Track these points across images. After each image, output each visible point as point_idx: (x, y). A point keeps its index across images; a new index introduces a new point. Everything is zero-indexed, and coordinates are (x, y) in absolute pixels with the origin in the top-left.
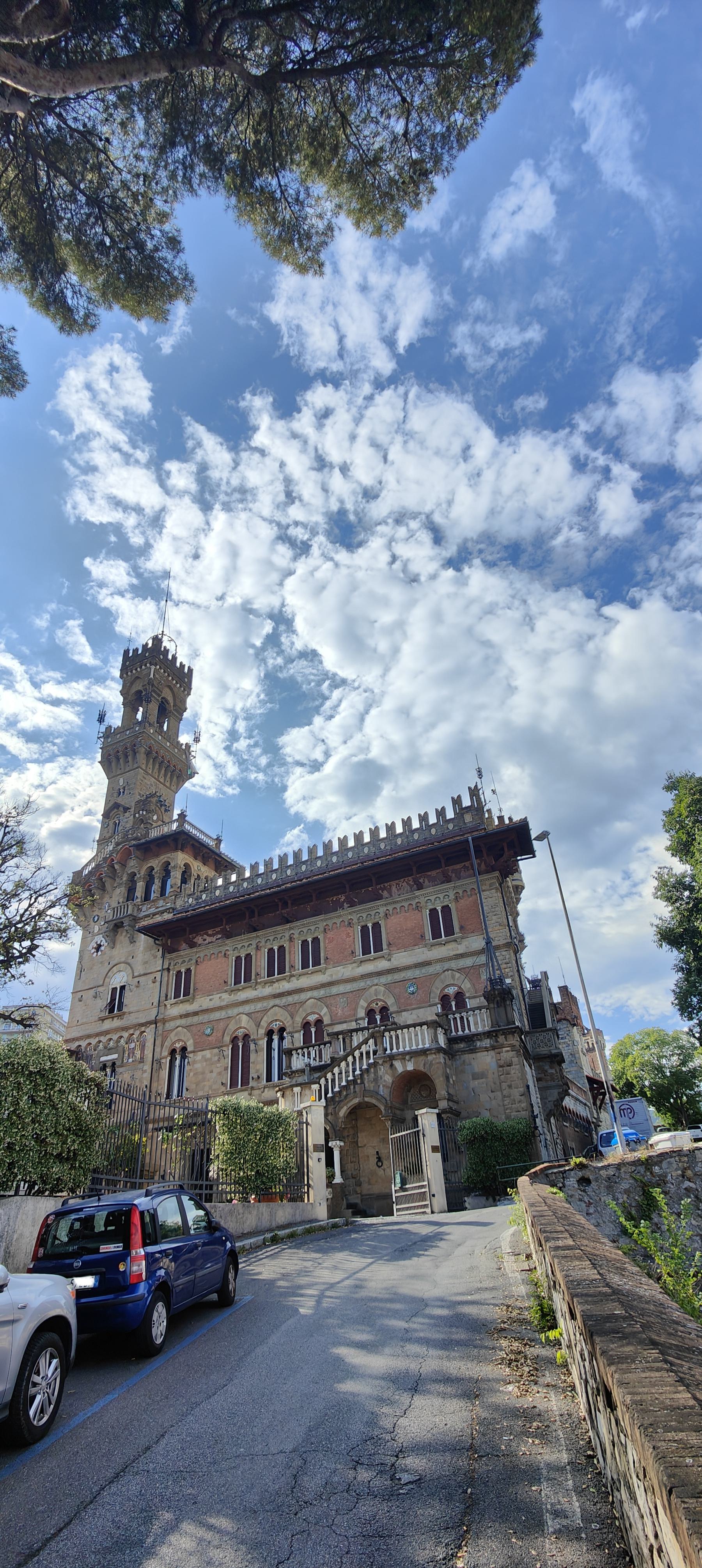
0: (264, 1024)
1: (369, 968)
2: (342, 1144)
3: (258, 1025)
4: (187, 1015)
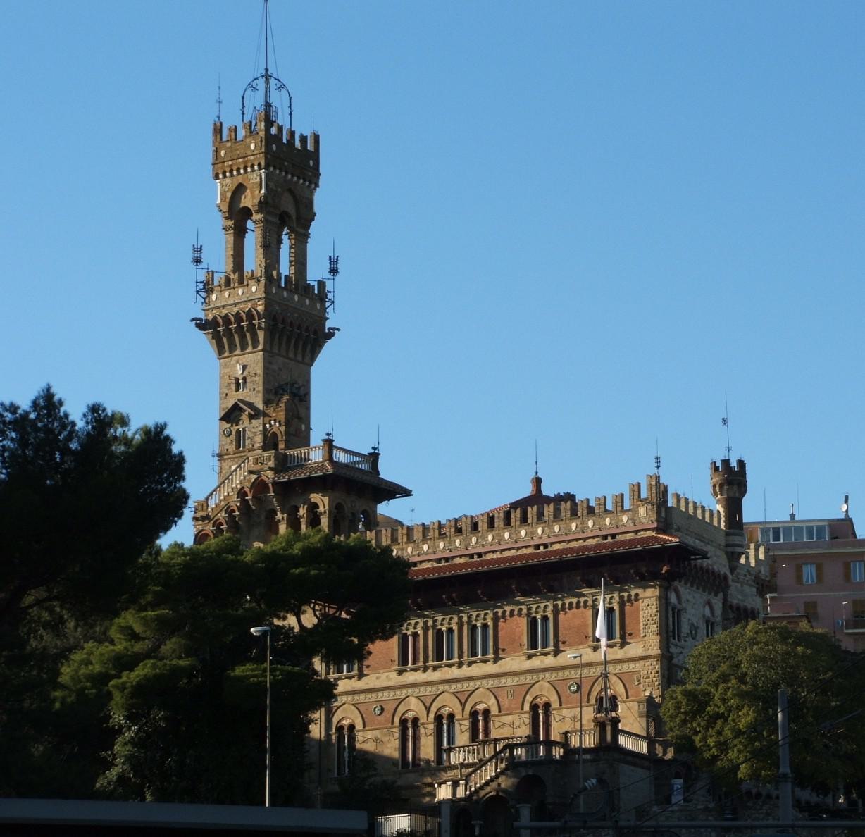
0: (434, 709)
1: (537, 662)
2: (481, 822)
3: (463, 705)
4: (353, 693)
